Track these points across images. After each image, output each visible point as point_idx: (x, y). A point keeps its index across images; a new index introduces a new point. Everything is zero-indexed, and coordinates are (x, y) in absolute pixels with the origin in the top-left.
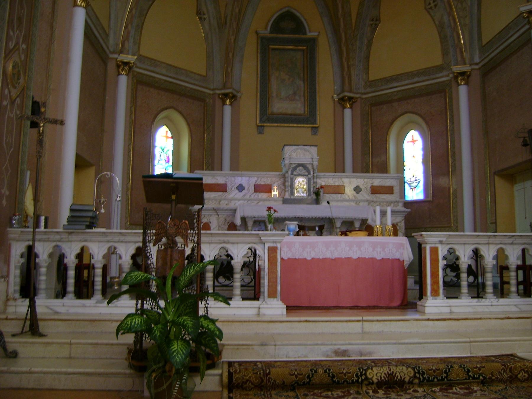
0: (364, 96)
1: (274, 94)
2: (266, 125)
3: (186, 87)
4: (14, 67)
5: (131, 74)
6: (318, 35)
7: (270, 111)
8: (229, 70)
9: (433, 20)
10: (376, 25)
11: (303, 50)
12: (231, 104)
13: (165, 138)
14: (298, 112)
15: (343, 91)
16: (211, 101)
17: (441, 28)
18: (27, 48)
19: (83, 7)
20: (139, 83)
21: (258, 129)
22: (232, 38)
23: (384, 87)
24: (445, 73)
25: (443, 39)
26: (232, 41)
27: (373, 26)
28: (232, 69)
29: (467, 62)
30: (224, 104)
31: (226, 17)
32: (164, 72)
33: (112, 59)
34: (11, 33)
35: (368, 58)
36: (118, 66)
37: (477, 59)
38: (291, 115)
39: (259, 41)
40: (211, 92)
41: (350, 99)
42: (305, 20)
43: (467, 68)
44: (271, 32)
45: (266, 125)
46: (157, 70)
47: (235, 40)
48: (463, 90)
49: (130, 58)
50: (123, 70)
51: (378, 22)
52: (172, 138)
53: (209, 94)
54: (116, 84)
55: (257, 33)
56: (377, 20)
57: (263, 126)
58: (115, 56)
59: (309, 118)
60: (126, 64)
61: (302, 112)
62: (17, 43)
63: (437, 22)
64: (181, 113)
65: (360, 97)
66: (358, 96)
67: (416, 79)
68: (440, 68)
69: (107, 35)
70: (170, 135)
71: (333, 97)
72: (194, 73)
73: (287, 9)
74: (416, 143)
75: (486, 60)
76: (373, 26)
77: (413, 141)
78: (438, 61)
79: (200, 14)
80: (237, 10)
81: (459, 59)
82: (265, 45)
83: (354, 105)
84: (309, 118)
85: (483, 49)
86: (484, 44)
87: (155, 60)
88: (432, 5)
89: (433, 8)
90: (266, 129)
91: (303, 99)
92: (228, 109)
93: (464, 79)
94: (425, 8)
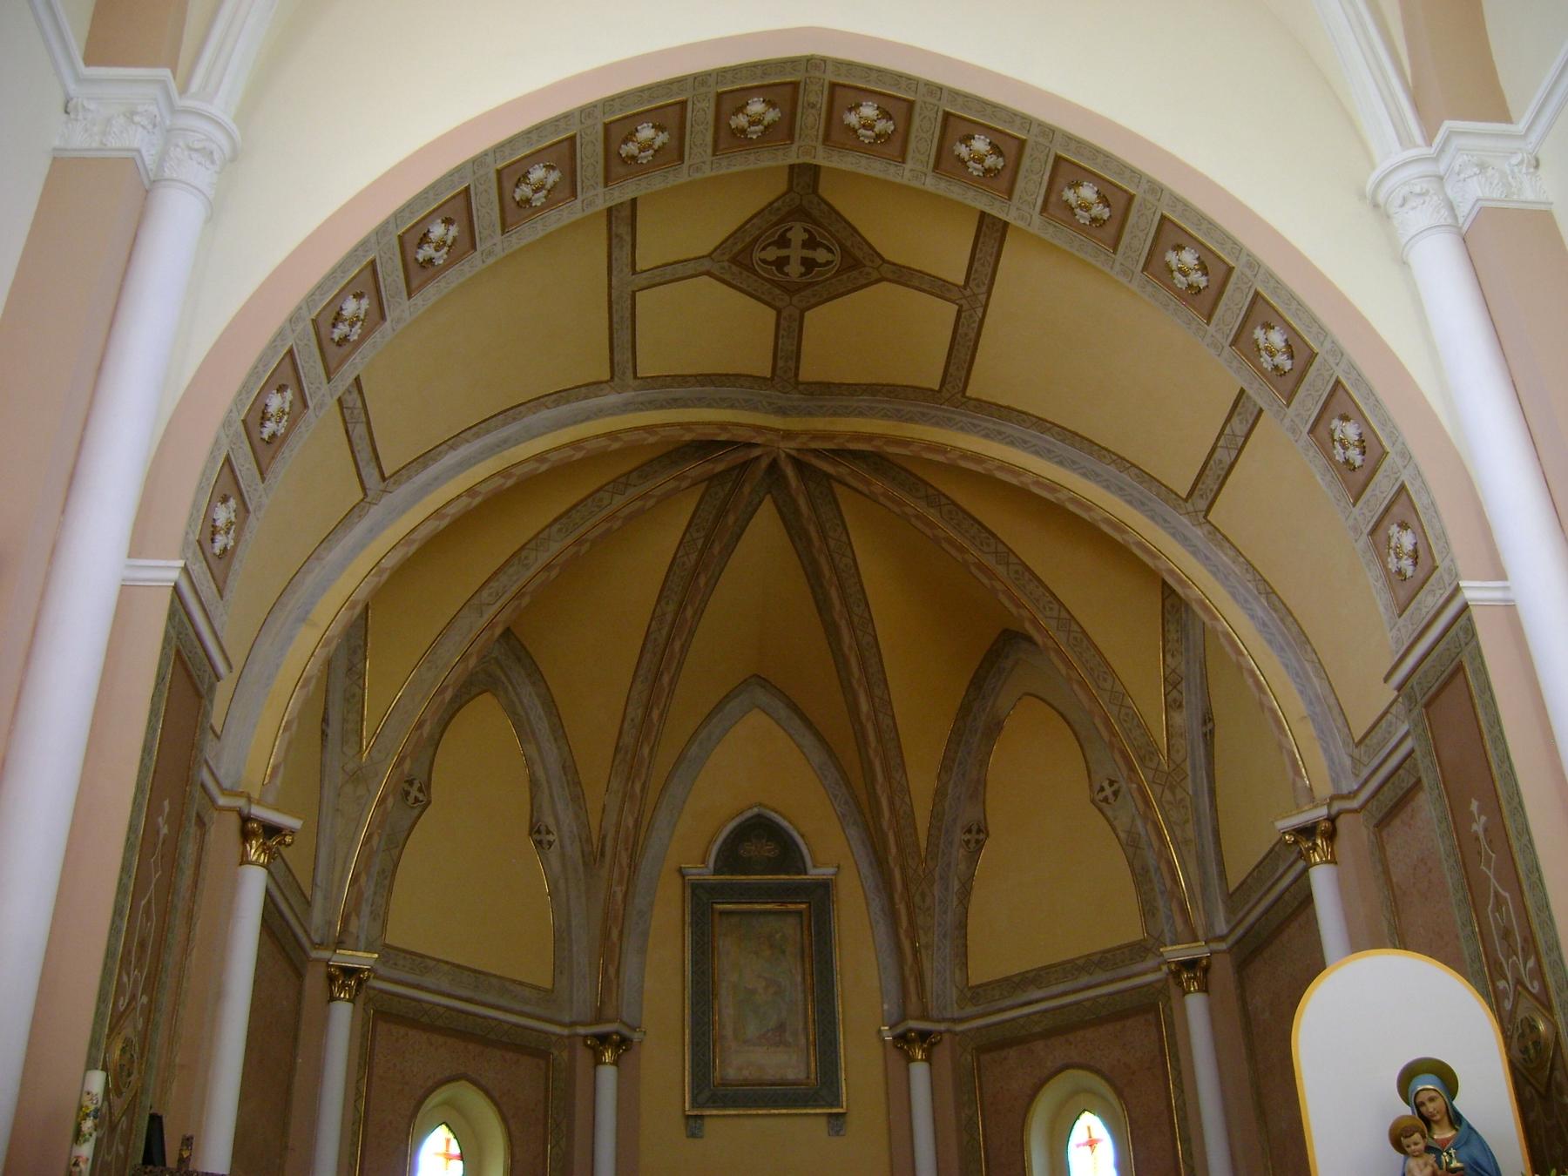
0: (960, 1028)
1: (728, 1032)
2: (707, 1112)
3: (500, 1021)
4: (123, 1050)
5: (362, 997)
6: (836, 874)
7: (717, 1075)
8: (612, 971)
9: (1114, 829)
10: (977, 842)
11: (800, 913)
12: (615, 1063)
13: (443, 1160)
14: (791, 1075)
15: (904, 1017)
16: (565, 1055)
17: (1132, 846)
18: (150, 1001)
19: (262, 865)
20: (385, 1016)
21: (687, 1125)
22: (619, 891)
23: (1008, 1002)
24: (1150, 962)
25: (1141, 876)
26: (620, 896)
27: (972, 845)
28: (618, 971)
29: (1200, 933)
30: (598, 1061)
31: (603, 839)
32: (445, 986)
33: (318, 960)
34: (125, 979)
35: (962, 926)
36: (331, 979)
37: (1221, 927)
38: (773, 1084)
39: (688, 892)
40: (566, 1032)
41: (924, 1036)
42: (802, 836)
43: (1199, 950)
44: (717, 871)
45: (707, 1112)
46: (428, 981)
47: (626, 895)
48: (1195, 1006)
49: (362, 959)
50: (342, 987)
51: (982, 836)
52: (461, 1157)
53: (561, 1036)
54: (324, 1021)
55: (681, 873)
56: (979, 831)
57: (701, 1117)
58: (326, 954)
59: (819, 1091)
60: (349, 972)
61: (802, 1076)
62: (133, 997)
63: (1123, 835)
64: (487, 1092)
65: (948, 1031)
66: (942, 1027)
67: (1084, 980)
68: (1139, 950)
69: (309, 904)
70: (455, 1149)
71: (880, 1031)
72: (521, 983)
73: (756, 810)
74: (1098, 1146)
75: (1240, 931)
76: (972, 845)
77: (1092, 1143)
78: (1133, 931)
79: (539, 832)
80: (631, 822)
81: (1180, 926)
82: (703, 903)
83: (936, 1049)
84: (819, 1091)
85: (1234, 899)
86: (1231, 889)
87: (422, 956)
88: (1108, 791)
89: (1111, 800)
90: (708, 1123)
91: (803, 1041)
92: (608, 1076)
93: (1195, 978)
94: (1093, 801)
